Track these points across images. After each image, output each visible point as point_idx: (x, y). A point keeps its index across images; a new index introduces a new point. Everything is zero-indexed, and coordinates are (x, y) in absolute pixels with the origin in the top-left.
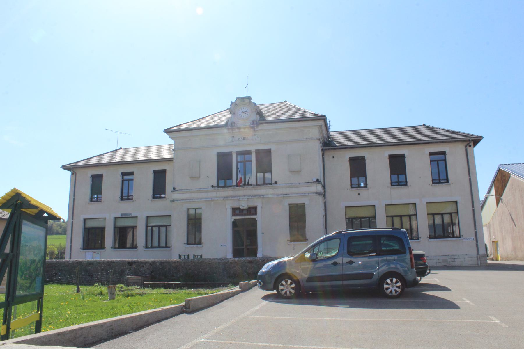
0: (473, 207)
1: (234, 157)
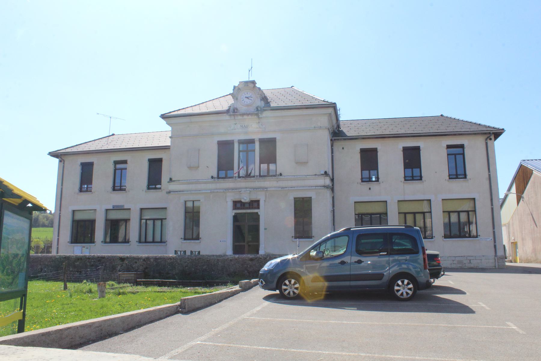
0: (492, 205)
1: (236, 145)
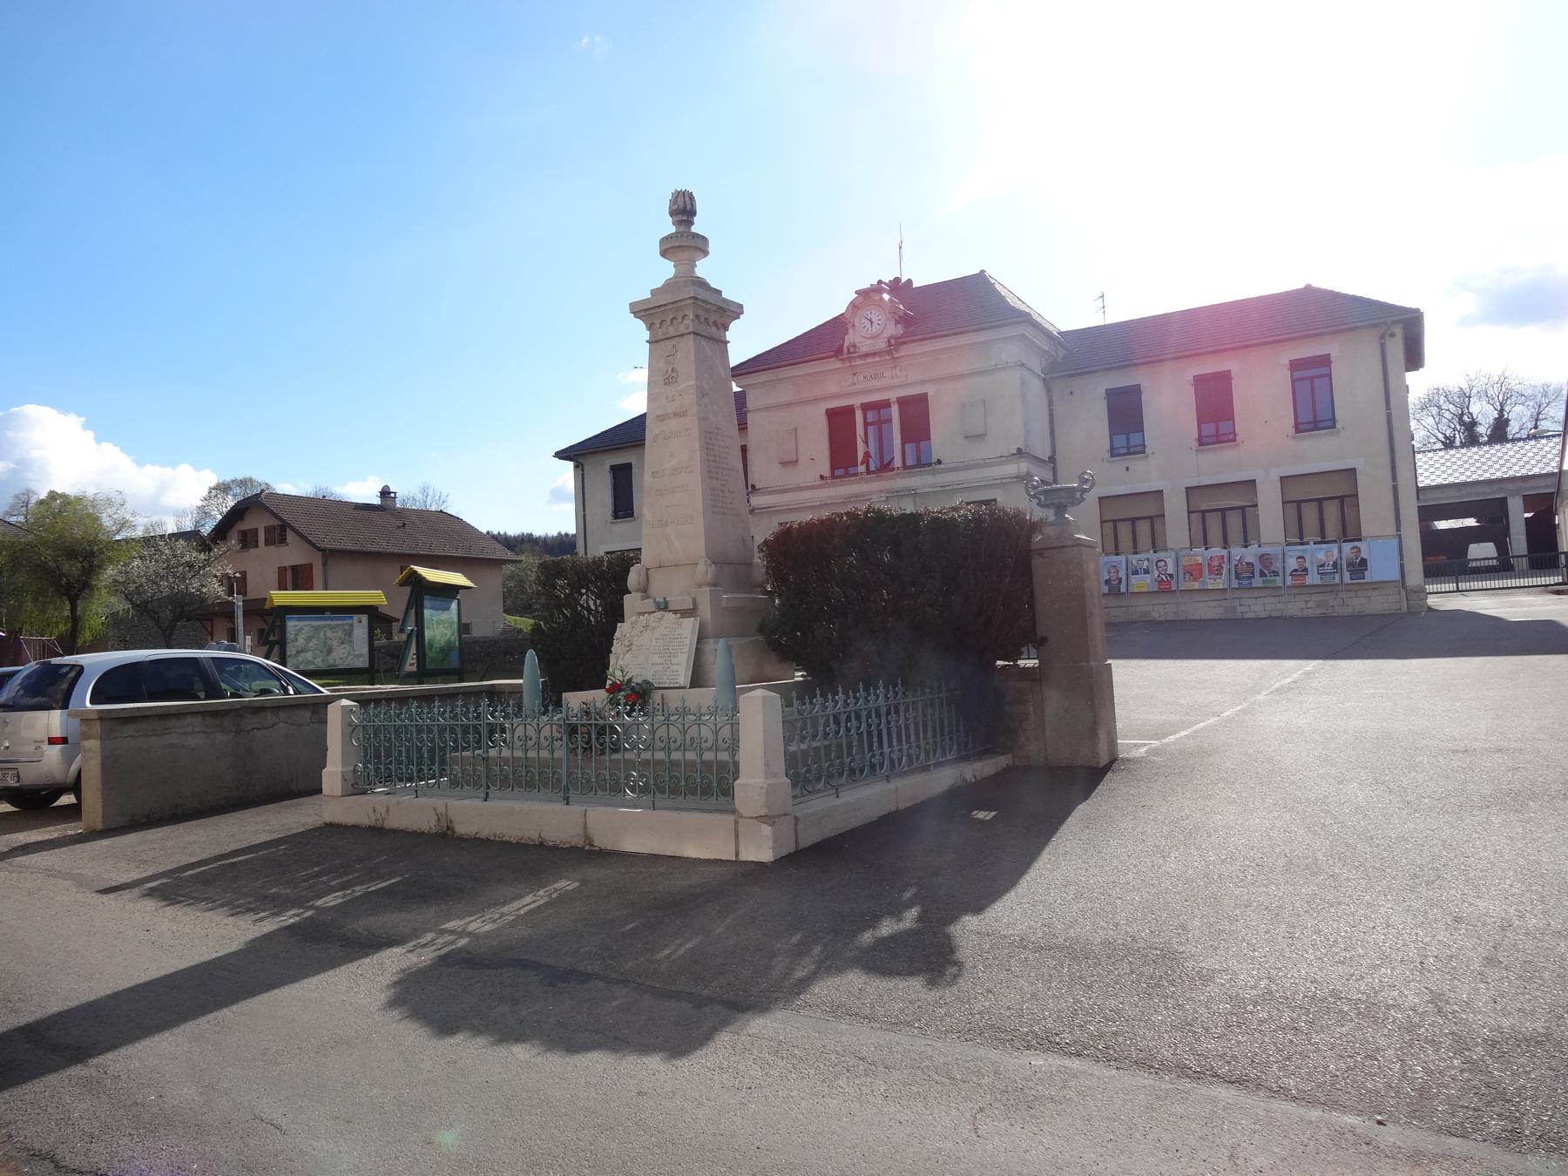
0: (1394, 478)
1: (859, 415)
